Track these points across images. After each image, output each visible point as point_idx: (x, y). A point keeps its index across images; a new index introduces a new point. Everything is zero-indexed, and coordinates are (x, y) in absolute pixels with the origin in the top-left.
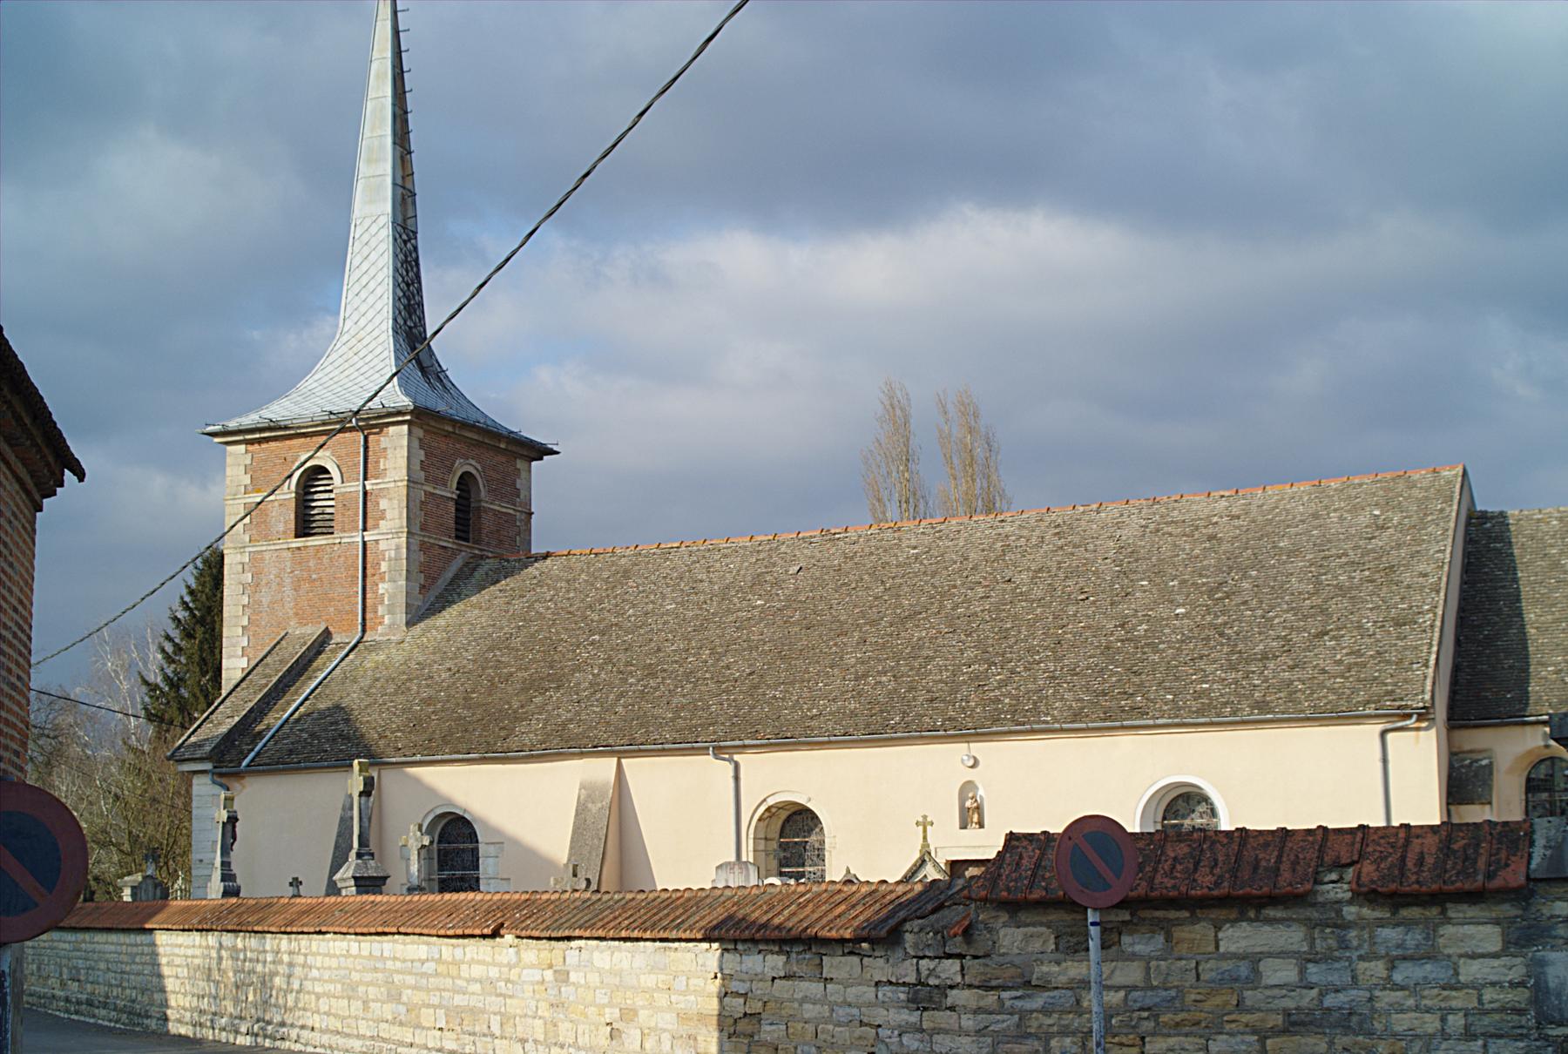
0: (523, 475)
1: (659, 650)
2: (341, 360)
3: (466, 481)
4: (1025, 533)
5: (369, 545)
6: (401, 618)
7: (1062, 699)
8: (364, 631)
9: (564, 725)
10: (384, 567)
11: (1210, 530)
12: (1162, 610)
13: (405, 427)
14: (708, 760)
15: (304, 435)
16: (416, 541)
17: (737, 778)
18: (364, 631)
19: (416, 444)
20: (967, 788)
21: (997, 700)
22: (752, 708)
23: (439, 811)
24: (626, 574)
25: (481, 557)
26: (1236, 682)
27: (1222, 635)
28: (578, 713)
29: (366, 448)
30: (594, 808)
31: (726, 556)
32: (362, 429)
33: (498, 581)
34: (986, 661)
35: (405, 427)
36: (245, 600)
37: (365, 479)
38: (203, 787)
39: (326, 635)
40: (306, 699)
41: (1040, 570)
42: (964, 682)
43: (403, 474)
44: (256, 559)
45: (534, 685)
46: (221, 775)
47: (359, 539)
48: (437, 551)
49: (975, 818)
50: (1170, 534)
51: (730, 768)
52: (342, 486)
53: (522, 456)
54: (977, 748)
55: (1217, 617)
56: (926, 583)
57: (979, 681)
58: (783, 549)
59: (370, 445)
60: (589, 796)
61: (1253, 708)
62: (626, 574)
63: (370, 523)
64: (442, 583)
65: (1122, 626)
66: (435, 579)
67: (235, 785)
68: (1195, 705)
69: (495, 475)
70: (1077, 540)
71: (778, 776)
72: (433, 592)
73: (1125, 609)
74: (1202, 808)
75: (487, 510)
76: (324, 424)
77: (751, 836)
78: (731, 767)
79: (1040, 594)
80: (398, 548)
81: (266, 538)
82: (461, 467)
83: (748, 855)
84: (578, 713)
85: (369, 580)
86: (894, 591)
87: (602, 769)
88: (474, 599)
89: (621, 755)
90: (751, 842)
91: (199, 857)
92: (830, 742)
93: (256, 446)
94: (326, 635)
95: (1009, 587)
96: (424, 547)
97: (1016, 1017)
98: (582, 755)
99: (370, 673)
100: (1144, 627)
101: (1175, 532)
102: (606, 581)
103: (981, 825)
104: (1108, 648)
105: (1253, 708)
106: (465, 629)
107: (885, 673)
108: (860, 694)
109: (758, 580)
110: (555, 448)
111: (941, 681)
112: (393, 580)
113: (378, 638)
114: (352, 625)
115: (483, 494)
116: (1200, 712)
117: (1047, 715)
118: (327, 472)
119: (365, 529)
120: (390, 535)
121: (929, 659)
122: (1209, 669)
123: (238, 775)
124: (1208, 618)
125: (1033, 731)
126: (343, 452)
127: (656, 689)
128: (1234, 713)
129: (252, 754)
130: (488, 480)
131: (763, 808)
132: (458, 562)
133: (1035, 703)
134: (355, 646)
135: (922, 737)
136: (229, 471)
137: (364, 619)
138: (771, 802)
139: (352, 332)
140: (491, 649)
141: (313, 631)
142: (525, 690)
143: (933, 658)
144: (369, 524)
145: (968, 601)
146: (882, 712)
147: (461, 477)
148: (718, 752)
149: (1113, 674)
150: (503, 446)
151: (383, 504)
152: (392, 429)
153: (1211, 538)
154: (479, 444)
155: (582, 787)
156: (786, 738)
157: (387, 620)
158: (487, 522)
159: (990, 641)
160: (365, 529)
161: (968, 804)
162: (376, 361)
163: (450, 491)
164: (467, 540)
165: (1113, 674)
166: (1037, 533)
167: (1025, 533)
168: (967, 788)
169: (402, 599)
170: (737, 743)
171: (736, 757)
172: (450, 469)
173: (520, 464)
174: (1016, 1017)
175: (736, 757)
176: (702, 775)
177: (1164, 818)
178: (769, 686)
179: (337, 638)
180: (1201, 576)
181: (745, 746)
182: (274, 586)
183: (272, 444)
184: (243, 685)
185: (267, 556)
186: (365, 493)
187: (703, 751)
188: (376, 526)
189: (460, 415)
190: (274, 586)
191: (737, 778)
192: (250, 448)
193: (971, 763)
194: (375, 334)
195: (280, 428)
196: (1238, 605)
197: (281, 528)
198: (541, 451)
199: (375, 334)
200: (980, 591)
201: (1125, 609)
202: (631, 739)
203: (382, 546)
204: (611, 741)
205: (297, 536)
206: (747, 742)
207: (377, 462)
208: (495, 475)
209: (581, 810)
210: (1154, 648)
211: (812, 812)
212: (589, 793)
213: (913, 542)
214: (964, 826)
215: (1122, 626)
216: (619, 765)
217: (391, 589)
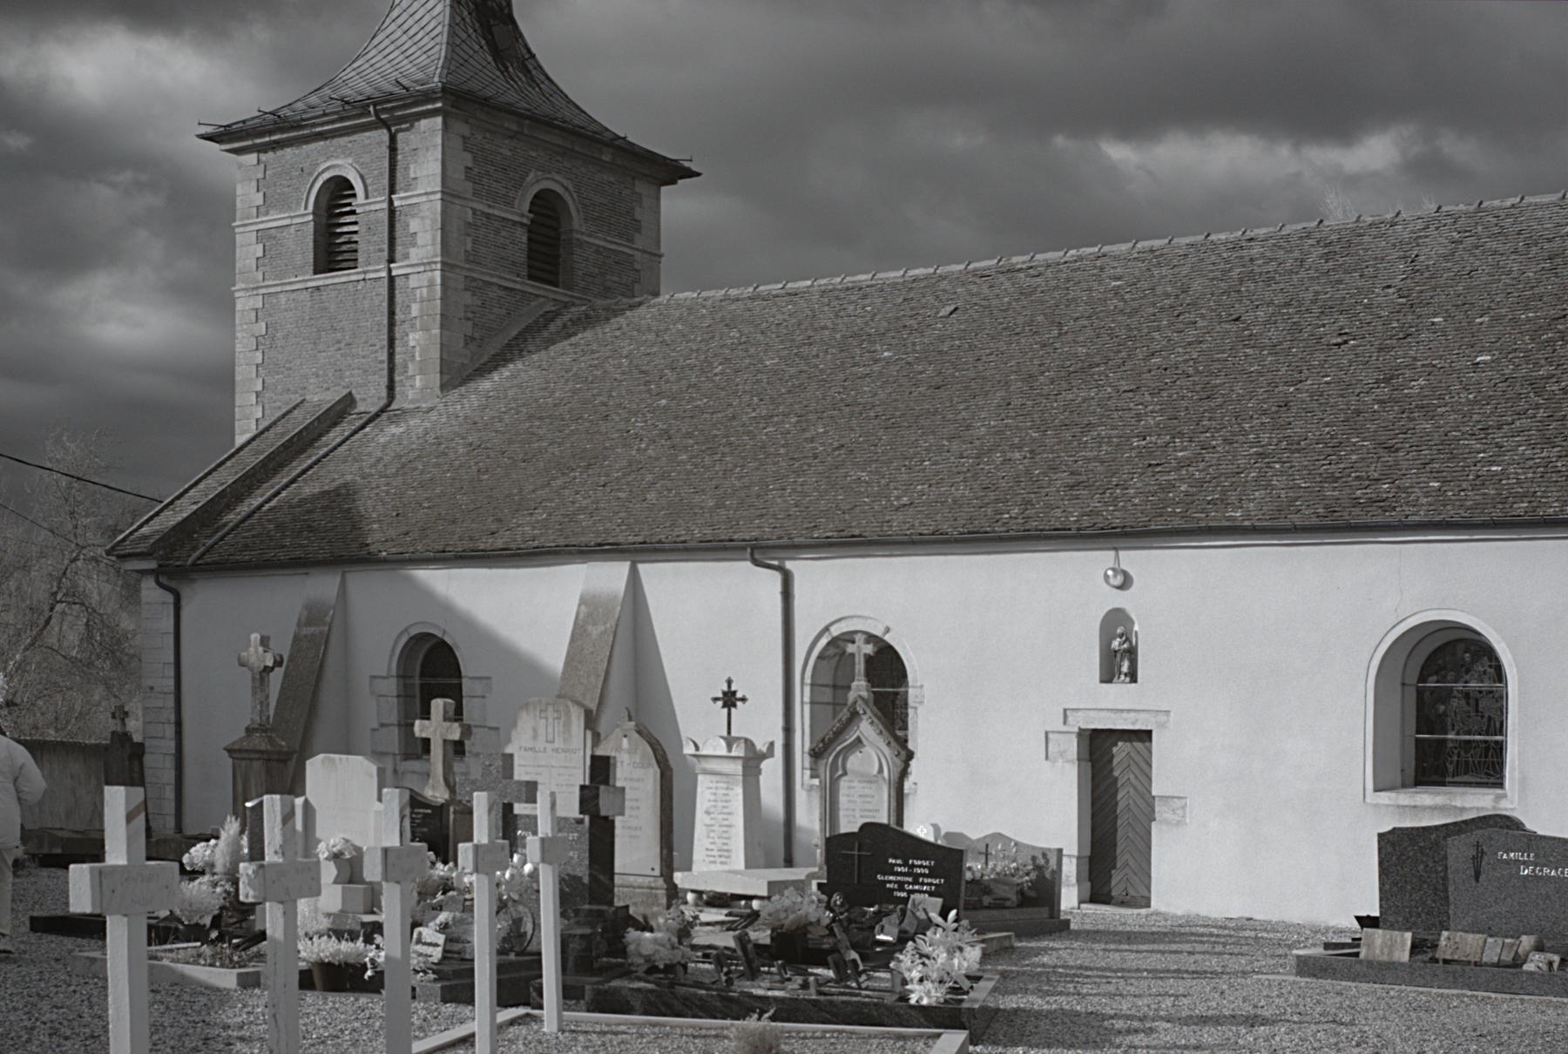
1: (734, 417)
3: (546, 204)
5: (399, 282)
6: (436, 379)
7: (1268, 486)
10: (415, 310)
13: (439, 120)
14: (742, 569)
19: (457, 143)
20: (1116, 625)
23: (414, 632)
30: (595, 631)
32: (385, 124)
35: (439, 120)
39: (348, 401)
47: (384, 274)
49: (1125, 669)
51: (777, 577)
52: (368, 204)
59: (400, 146)
60: (590, 615)
63: (399, 249)
65: (1387, 380)
71: (849, 593)
77: (808, 680)
80: (431, 284)
82: (536, 183)
86: (1070, 337)
87: (610, 576)
88: (535, 357)
90: (807, 690)
91: (150, 682)
96: (472, 286)
97: (596, 965)
101: (1501, 248)
103: (1133, 677)
104: (1358, 412)
107: (1020, 448)
110: (694, 168)
112: (425, 329)
115: (577, 222)
118: (352, 188)
131: (824, 641)
133: (1224, 493)
140: (530, 417)
141: (322, 397)
144: (398, 255)
146: (997, 501)
149: (1356, 449)
150: (606, 158)
151: (414, 225)
152: (423, 124)
161: (1115, 644)
162: (426, 39)
165: (1356, 449)
168: (1116, 625)
171: (789, 565)
173: (640, 187)
174: (596, 965)
179: (361, 407)
186: (392, 211)
192: (263, 157)
193: (1119, 580)
195: (293, 128)
197: (298, 260)
198: (674, 172)
203: (413, 282)
205: (316, 272)
207: (407, 169)
211: (896, 653)
212: (590, 608)
215: (1387, 380)
217: (421, 340)
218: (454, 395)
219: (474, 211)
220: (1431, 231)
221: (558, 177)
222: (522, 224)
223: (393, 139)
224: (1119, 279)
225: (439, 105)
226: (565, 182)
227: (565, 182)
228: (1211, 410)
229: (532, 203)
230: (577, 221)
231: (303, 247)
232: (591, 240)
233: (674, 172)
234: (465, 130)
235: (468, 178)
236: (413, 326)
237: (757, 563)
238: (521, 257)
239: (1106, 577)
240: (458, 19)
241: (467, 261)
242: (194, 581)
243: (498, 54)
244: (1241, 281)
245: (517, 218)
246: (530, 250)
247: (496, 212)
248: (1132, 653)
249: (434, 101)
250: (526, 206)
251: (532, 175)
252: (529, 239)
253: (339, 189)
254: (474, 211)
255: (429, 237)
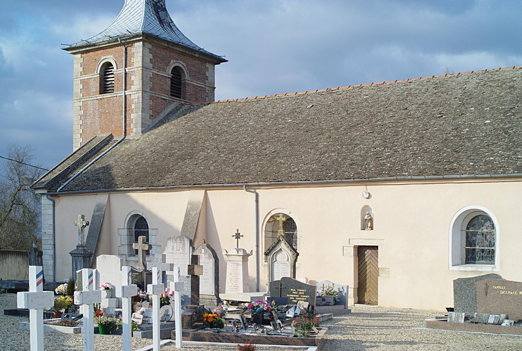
0: (210, 70)
2: (124, 17)
3: (177, 71)
4: (420, 87)
5: (127, 97)
6: (140, 129)
8: (125, 135)
9: (185, 175)
10: (133, 106)
11: (511, 84)
12: (478, 122)
13: (141, 43)
14: (243, 192)
15: (102, 48)
16: (147, 96)
17: (257, 201)
18: (125, 135)
19: (147, 51)
20: (366, 209)
21: (384, 164)
22: (268, 167)
23: (133, 214)
24: (239, 110)
25: (183, 105)
26: (509, 156)
27: (506, 133)
28: (194, 170)
29: (126, 53)
30: (193, 213)
31: (283, 101)
32: (124, 44)
33: (186, 114)
34: (383, 146)
35: (141, 43)
36: (81, 122)
37: (126, 67)
38: (45, 201)
39: (111, 137)
40: (92, 164)
41: (422, 104)
42: (371, 156)
43: (140, 64)
44: (85, 104)
45: (182, 158)
46: (52, 195)
47: (123, 94)
48: (160, 101)
49: (369, 225)
50: (491, 86)
51: (254, 195)
52: (117, 71)
53: (209, 62)
54: (372, 189)
55: (506, 124)
56: (367, 110)
57: (377, 156)
58: (308, 98)
59: (128, 51)
60: (191, 208)
61: (515, 170)
62: (239, 110)
63: (128, 86)
64: (162, 115)
65: (456, 129)
66: (158, 113)
67: (57, 200)
68: (484, 168)
69: (194, 69)
70: (443, 90)
71: (279, 200)
72: (155, 117)
73: (460, 121)
74: (488, 224)
75: (188, 84)
76: (109, 43)
77: (264, 230)
78: (254, 195)
79: (419, 114)
81: (89, 95)
82: (173, 63)
83: (126, 227)
84: (194, 170)
85: (127, 112)
87: (198, 195)
88: (173, 122)
89: (207, 189)
90: (264, 232)
92: (299, 184)
93: (85, 55)
94: (111, 137)
95: (405, 112)
96: (152, 98)
98: (189, 188)
99: (121, 153)
100: (467, 129)
101: (493, 85)
102: (229, 113)
103: (372, 229)
104: (446, 140)
105: (515, 170)
106: (165, 134)
107: (334, 152)
108: (319, 161)
109: (293, 111)
111: (360, 155)
113: (130, 138)
114: (121, 133)
116: (486, 172)
117: (406, 172)
119: (126, 90)
120: (135, 92)
121: (357, 145)
122: (495, 150)
123: (57, 196)
124: (501, 125)
125: (397, 180)
126: (117, 55)
127: (230, 159)
128: (504, 172)
129: (62, 186)
130: (190, 71)
132: (172, 107)
133: (402, 166)
134: (121, 142)
135: (342, 182)
136: (75, 67)
137: (125, 130)
138: (273, 213)
139: (130, 5)
140: (171, 142)
141: (106, 135)
142: (177, 159)
143: (359, 144)
144: (127, 88)
145: (384, 118)
146: (327, 169)
147: (174, 68)
148: (248, 188)
151: (133, 78)
152: (136, 44)
153: (510, 87)
154: (184, 54)
155: (189, 203)
156: (279, 181)
157: (134, 131)
158: (189, 90)
159: (388, 137)
160: (126, 90)
161: (366, 217)
163: (168, 72)
164: (180, 98)
166: (426, 87)
167: (420, 87)
168: (366, 209)
169: (140, 121)
170: (256, 183)
171: (257, 191)
172: (168, 64)
173: (208, 65)
175: (257, 191)
176: (242, 198)
177: (468, 228)
178: (280, 158)
179: (115, 139)
180: (502, 105)
181: (260, 185)
182: (92, 116)
183: (91, 53)
184: (71, 158)
185: (89, 102)
186: (126, 74)
187: (240, 187)
188: (130, 88)
189: (176, 40)
190: (92, 116)
191: (257, 201)
192: (83, 55)
193: (367, 196)
194: (138, 5)
196: (517, 119)
198: (219, 60)
199: (138, 5)
200: (391, 113)
201: (460, 121)
202: (209, 183)
203: (133, 97)
204: (202, 182)
206: (260, 183)
207: (131, 59)
208: (194, 69)
209: (187, 215)
210: (469, 139)
212: (191, 207)
213: (367, 93)
214: (363, 229)
215: (456, 129)
216: (206, 193)
217: (136, 116)
218: (146, 135)
219: (153, 73)
220: (470, 80)
221: (181, 62)
222: (169, 78)
223: (126, 49)
224: (367, 95)
225: (141, 38)
226: (183, 64)
227: (183, 64)
228: (398, 139)
229: (172, 71)
230: (187, 77)
231: (95, 86)
232: (192, 83)
233: (219, 60)
234: (150, 46)
235: (151, 62)
236: (133, 112)
237: (247, 190)
238: (168, 88)
239: (363, 195)
240: (148, 9)
241: (151, 90)
242: (61, 198)
243: (161, 21)
244: (407, 96)
245: (167, 76)
246: (171, 86)
247: (160, 74)
248: (371, 220)
249: (140, 36)
250: (170, 72)
251: (172, 61)
252: (171, 83)
253: (108, 66)
254: (153, 73)
255: (138, 81)
